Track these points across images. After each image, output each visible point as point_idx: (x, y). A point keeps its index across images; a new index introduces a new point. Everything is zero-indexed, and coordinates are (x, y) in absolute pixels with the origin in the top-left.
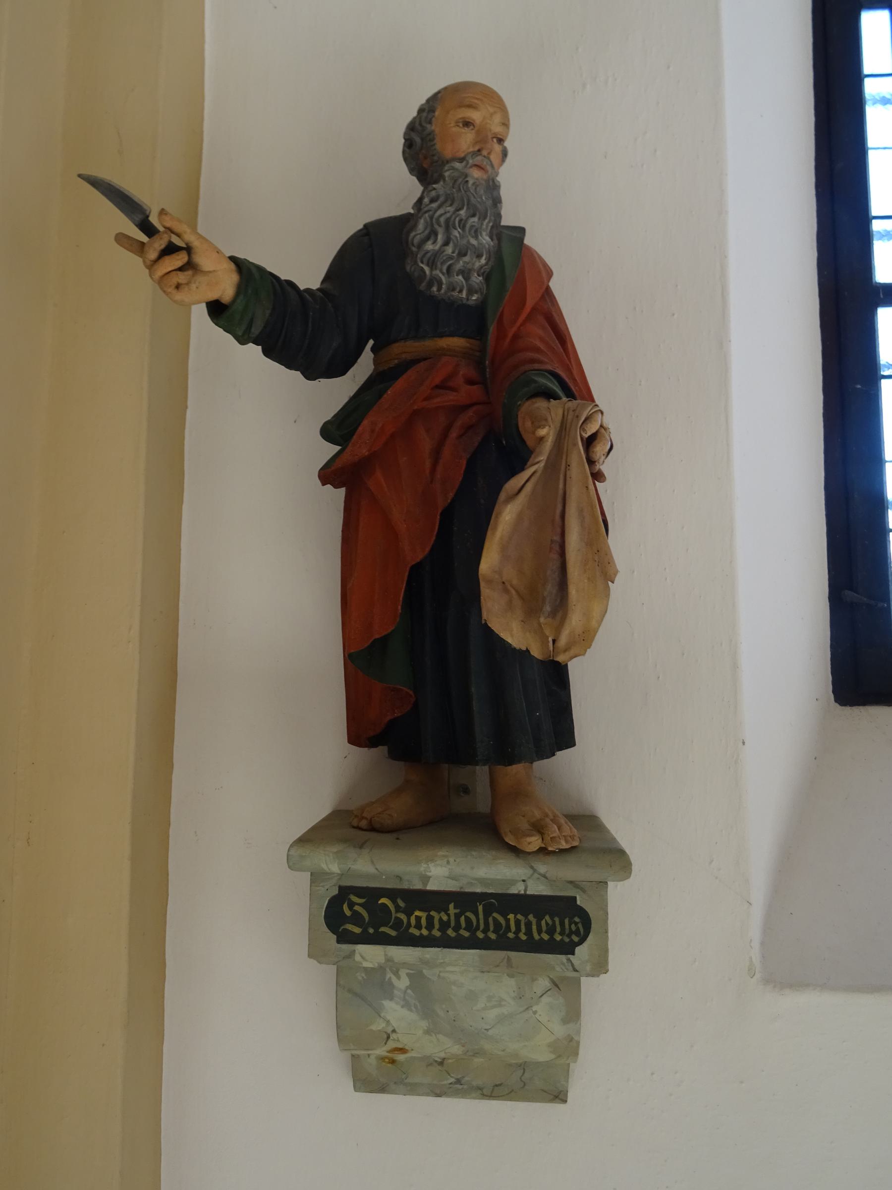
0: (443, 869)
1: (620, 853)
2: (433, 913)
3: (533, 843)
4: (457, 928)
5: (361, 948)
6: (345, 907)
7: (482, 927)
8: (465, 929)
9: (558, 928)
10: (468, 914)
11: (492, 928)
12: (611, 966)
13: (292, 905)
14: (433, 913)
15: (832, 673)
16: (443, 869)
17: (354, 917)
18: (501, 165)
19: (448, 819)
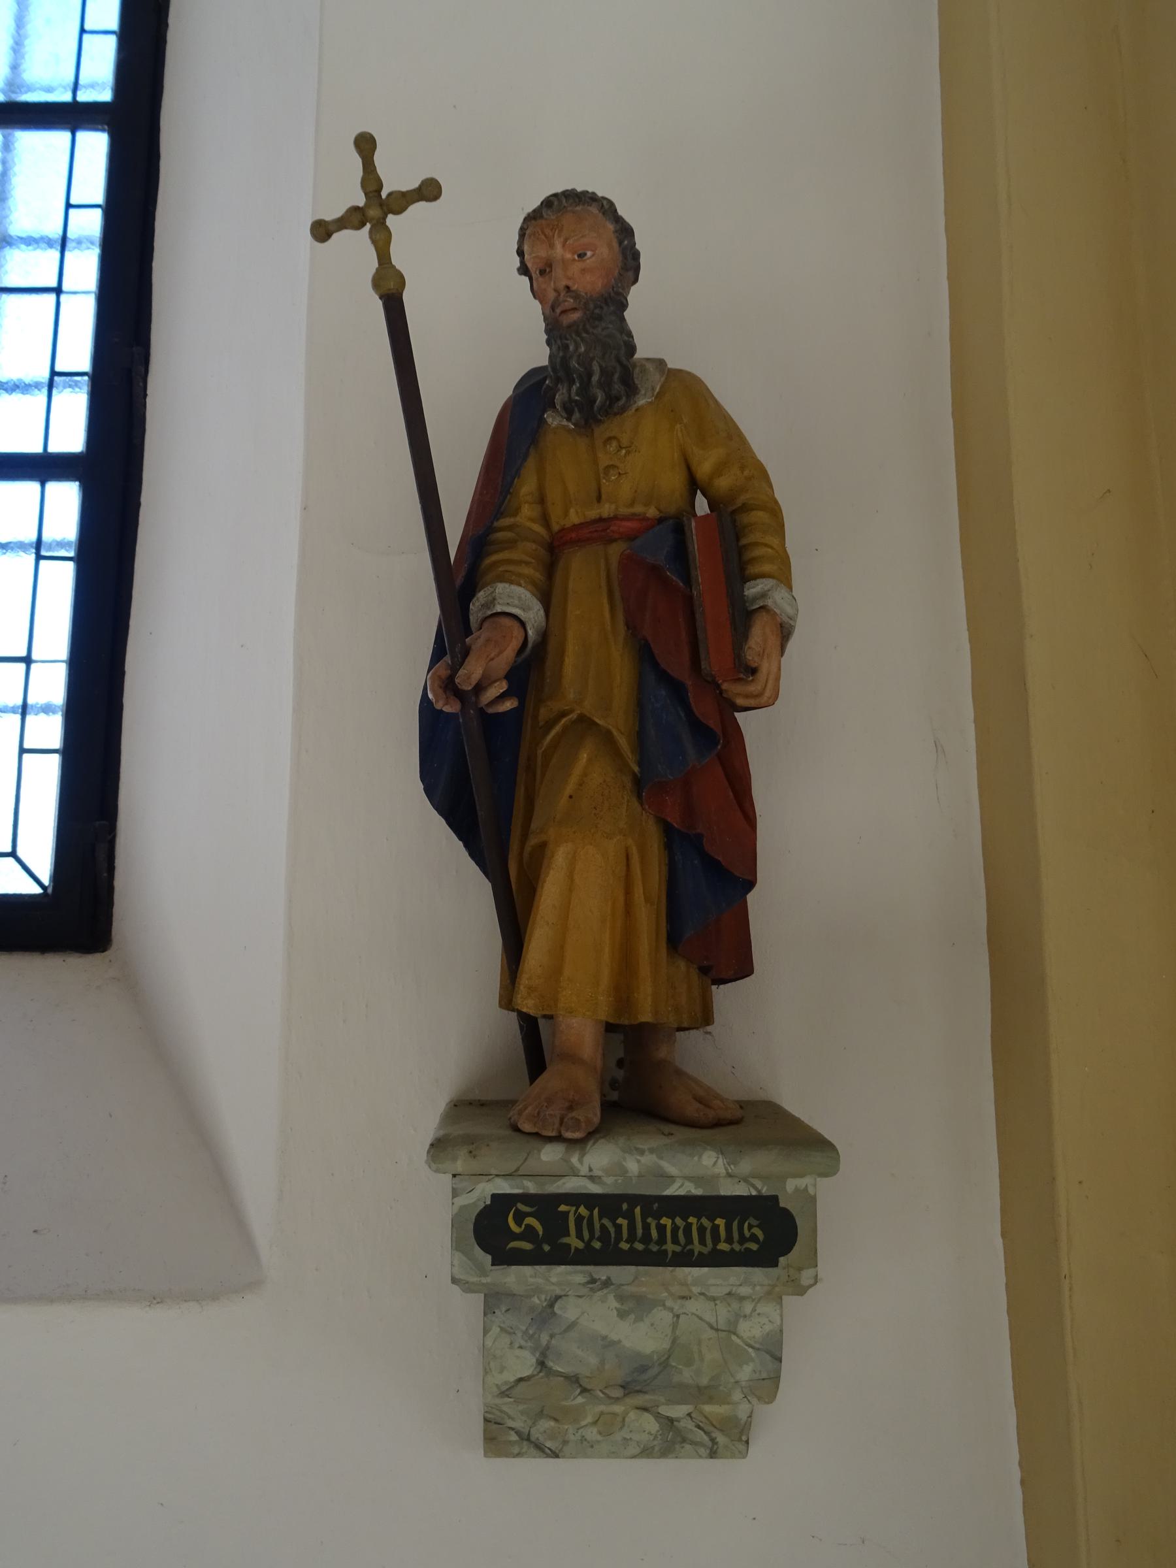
0: (608, 1165)
8: (627, 1241)
16: (608, 1165)
17: (505, 1233)
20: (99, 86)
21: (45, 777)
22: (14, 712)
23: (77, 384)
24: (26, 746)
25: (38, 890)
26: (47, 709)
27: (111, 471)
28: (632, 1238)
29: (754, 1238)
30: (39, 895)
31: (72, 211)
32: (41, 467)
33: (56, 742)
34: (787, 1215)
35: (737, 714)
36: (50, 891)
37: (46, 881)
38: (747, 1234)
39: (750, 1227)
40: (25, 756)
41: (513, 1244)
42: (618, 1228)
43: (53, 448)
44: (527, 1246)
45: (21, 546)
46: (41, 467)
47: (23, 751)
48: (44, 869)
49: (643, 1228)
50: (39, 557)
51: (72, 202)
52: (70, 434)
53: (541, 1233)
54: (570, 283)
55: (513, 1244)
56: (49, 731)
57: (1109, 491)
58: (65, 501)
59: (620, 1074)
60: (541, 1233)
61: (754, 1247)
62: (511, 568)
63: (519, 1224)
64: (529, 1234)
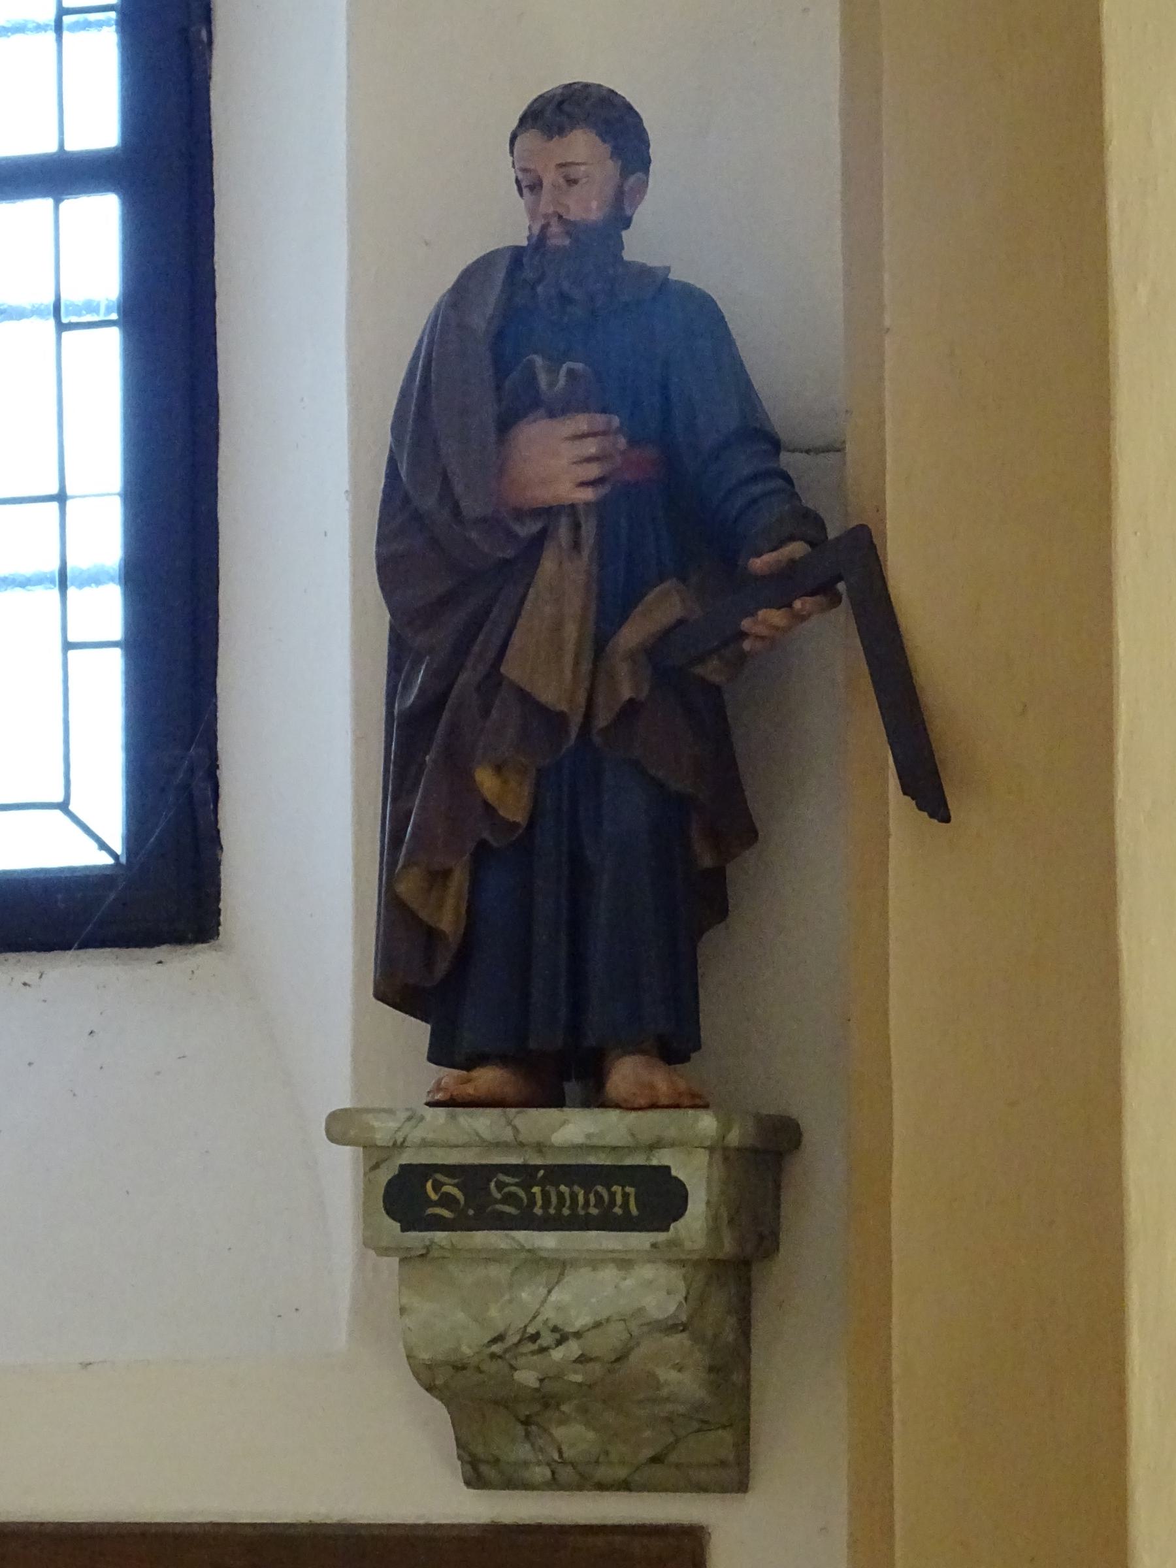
2: (563, 1188)
6: (429, 1185)
8: (595, 1206)
17: (411, 1198)
21: (104, 684)
22: (109, 25)
23: (100, 24)
24: (71, 638)
25: (110, 861)
26: (94, 579)
30: (106, 867)
32: (57, 175)
33: (115, 629)
36: (123, 860)
37: (118, 847)
40: (71, 654)
41: (430, 1211)
43: (72, 146)
44: (446, 1213)
45: (37, 312)
46: (57, 175)
47: (68, 646)
48: (115, 833)
50: (61, 327)
54: (561, 211)
55: (430, 1211)
56: (104, 611)
57: (25, 984)
58: (97, 224)
59: (572, 1088)
64: (447, 1201)
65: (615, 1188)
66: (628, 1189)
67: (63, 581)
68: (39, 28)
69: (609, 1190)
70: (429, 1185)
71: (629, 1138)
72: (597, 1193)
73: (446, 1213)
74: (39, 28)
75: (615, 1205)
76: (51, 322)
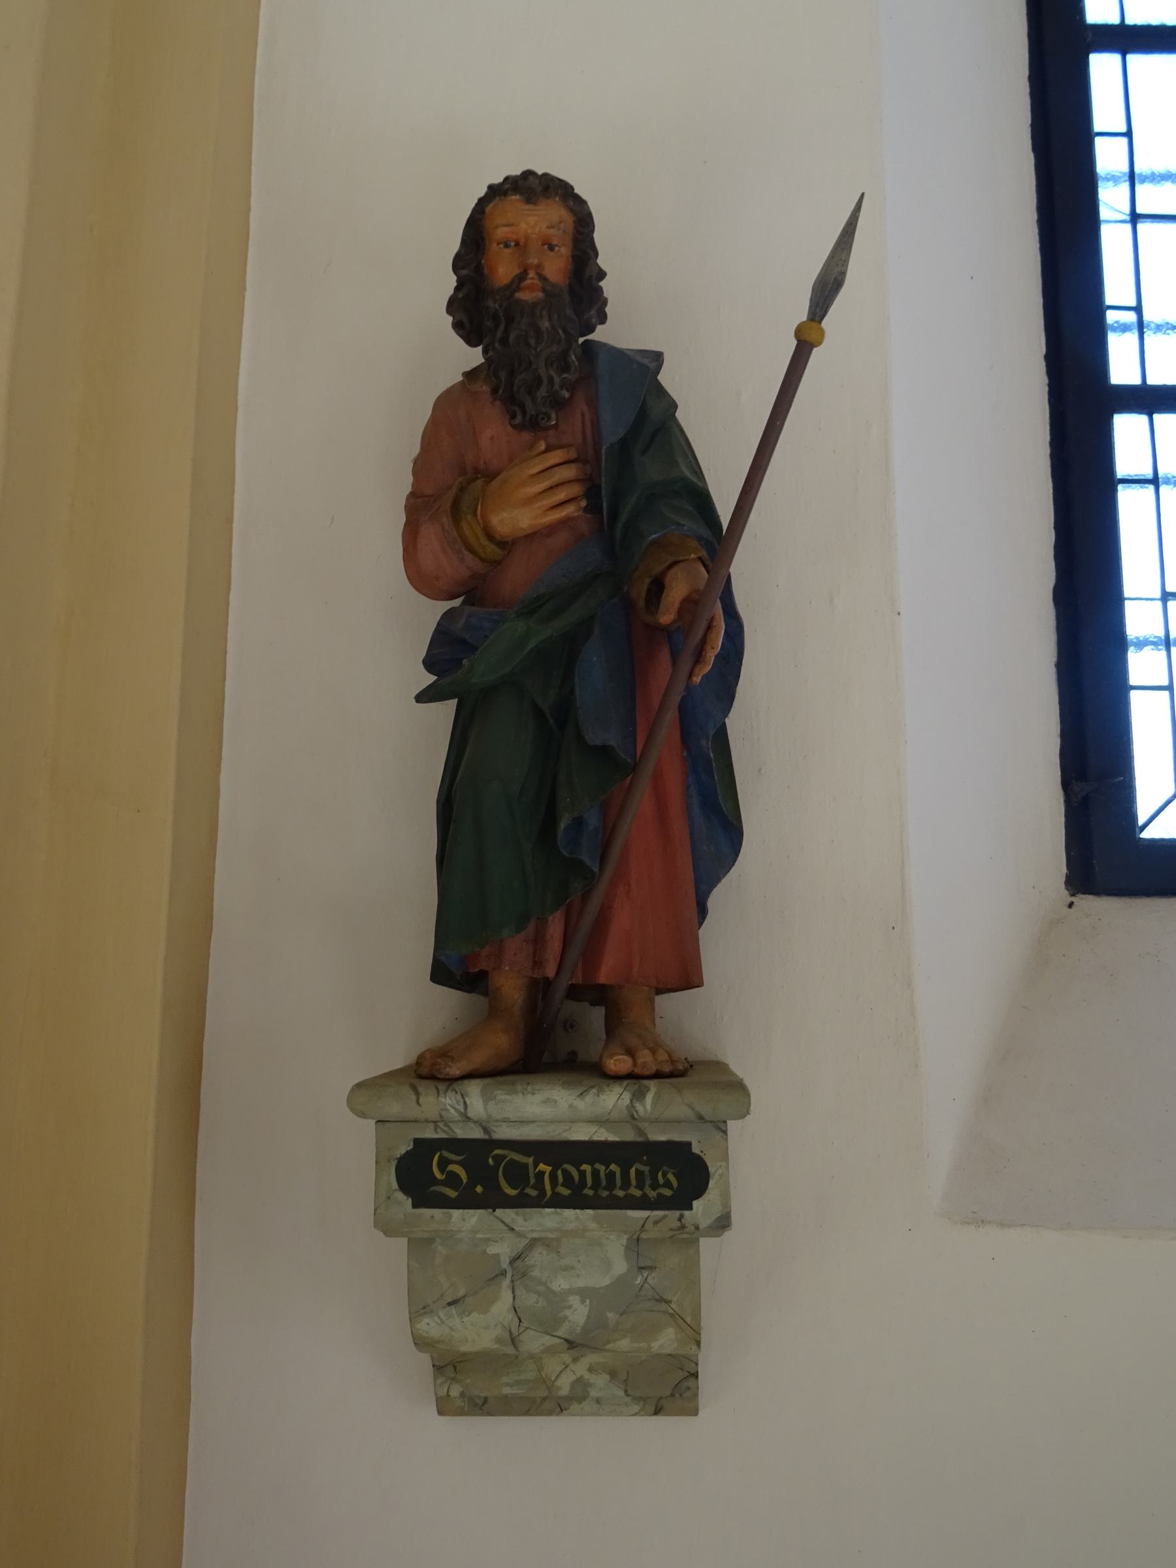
0: (546, 1110)
1: (738, 1087)
2: (584, 1167)
3: (618, 1063)
4: (626, 1185)
5: (456, 1214)
6: (660, 1174)
7: (589, 1182)
8: (591, 1188)
9: (668, 1177)
10: (566, 1166)
11: (634, 1182)
12: (442, 1418)
13: (355, 1157)
14: (597, 1166)
15: (1034, 150)
16: (546, 1110)
17: (435, 1174)
18: (701, 924)
19: (540, 1053)
20: (1103, 68)
27: (1082, 405)
28: (596, 1184)
29: (668, 1184)
31: (1124, 129)
32: (1152, 400)
34: (404, 1186)
35: (456, 700)
38: (661, 1180)
39: (664, 1175)
40: (1166, 683)
42: (582, 1174)
44: (452, 1194)
46: (1152, 400)
47: (1129, 134)
49: (628, 1174)
51: (1125, 140)
52: (1129, 432)
53: (465, 1181)
60: (465, 1181)
61: (668, 1192)
62: (502, 327)
63: (442, 1168)
64: (452, 1180)
65: (584, 1167)
66: (613, 1167)
67: (1155, 481)
68: (1159, 328)
69: (579, 1170)
70: (660, 1174)
71: (420, 1089)
72: (565, 1172)
73: (452, 1194)
74: (1159, 328)
75: (586, 1186)
76: (1147, 317)
